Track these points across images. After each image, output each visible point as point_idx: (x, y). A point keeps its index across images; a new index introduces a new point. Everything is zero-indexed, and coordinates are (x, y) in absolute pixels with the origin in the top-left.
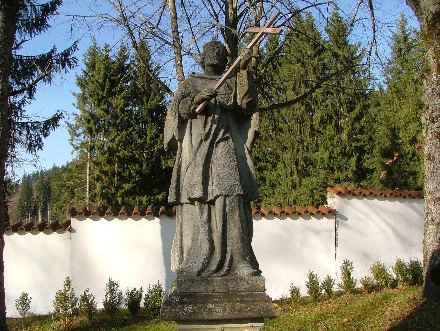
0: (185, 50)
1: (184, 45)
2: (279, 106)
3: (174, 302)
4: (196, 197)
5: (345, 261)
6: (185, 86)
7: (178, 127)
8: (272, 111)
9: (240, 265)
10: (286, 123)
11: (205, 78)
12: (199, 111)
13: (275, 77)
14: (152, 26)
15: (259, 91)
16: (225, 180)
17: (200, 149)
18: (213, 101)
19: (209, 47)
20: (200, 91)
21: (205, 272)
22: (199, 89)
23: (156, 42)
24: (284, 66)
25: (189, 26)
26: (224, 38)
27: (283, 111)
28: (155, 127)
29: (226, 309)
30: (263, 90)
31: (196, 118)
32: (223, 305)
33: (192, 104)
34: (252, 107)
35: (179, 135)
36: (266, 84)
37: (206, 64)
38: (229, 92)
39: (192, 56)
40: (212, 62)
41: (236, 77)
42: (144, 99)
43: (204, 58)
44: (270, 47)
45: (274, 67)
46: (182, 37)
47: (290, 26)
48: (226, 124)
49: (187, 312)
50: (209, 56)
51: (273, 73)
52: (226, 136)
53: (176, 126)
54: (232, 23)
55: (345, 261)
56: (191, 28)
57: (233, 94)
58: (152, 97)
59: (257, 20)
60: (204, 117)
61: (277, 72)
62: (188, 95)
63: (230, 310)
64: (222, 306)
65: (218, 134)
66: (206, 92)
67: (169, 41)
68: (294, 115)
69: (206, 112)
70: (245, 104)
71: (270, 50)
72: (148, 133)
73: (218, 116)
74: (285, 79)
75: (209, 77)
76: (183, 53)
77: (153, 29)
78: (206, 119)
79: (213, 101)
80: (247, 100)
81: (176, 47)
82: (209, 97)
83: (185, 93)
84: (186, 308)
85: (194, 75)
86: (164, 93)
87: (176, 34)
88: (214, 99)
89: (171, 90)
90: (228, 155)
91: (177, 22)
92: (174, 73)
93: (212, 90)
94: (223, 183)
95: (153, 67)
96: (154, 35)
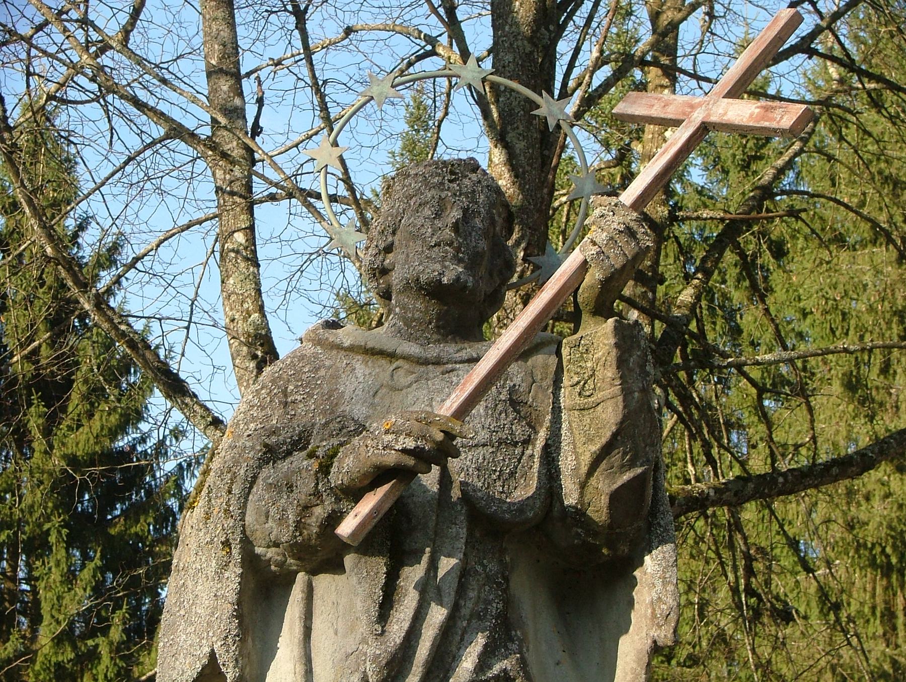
0: (274, 176)
1: (265, 144)
2: (769, 487)
6: (285, 393)
7: (239, 615)
8: (734, 515)
10: (809, 570)
11: (391, 356)
12: (354, 534)
13: (750, 319)
14: (94, 36)
15: (669, 405)
18: (430, 480)
19: (418, 192)
20: (361, 428)
22: (359, 411)
23: (117, 122)
24: (804, 259)
25: (298, 43)
26: (486, 114)
27: (792, 509)
28: (86, 575)
30: (686, 399)
31: (337, 567)
33: (317, 494)
34: (643, 516)
35: (242, 656)
36: (705, 358)
37: (396, 279)
38: (520, 431)
39: (309, 206)
40: (430, 271)
41: (558, 354)
42: (34, 422)
43: (389, 249)
44: (726, 154)
45: (748, 266)
46: (260, 102)
47: (837, 52)
48: (496, 607)
50: (414, 237)
51: (738, 296)
52: (496, 669)
53: (228, 609)
54: (531, 40)
56: (308, 53)
57: (540, 443)
58: (75, 401)
59: (664, 20)
60: (379, 566)
61: (760, 293)
62: (300, 443)
65: (456, 659)
66: (397, 433)
67: (189, 123)
68: (850, 526)
69: (392, 540)
70: (604, 500)
71: (726, 172)
72: (45, 608)
73: (453, 561)
74: (805, 327)
75: (412, 349)
76: (259, 188)
77: (103, 50)
78: (392, 577)
79: (430, 480)
80: (611, 476)
81: (224, 155)
82: (410, 461)
83: (284, 436)
85: (334, 336)
86: (144, 390)
87: (225, 85)
88: (435, 470)
89: (194, 387)
91: (232, 26)
92: (211, 291)
93: (428, 420)
95: (89, 245)
96: (107, 86)
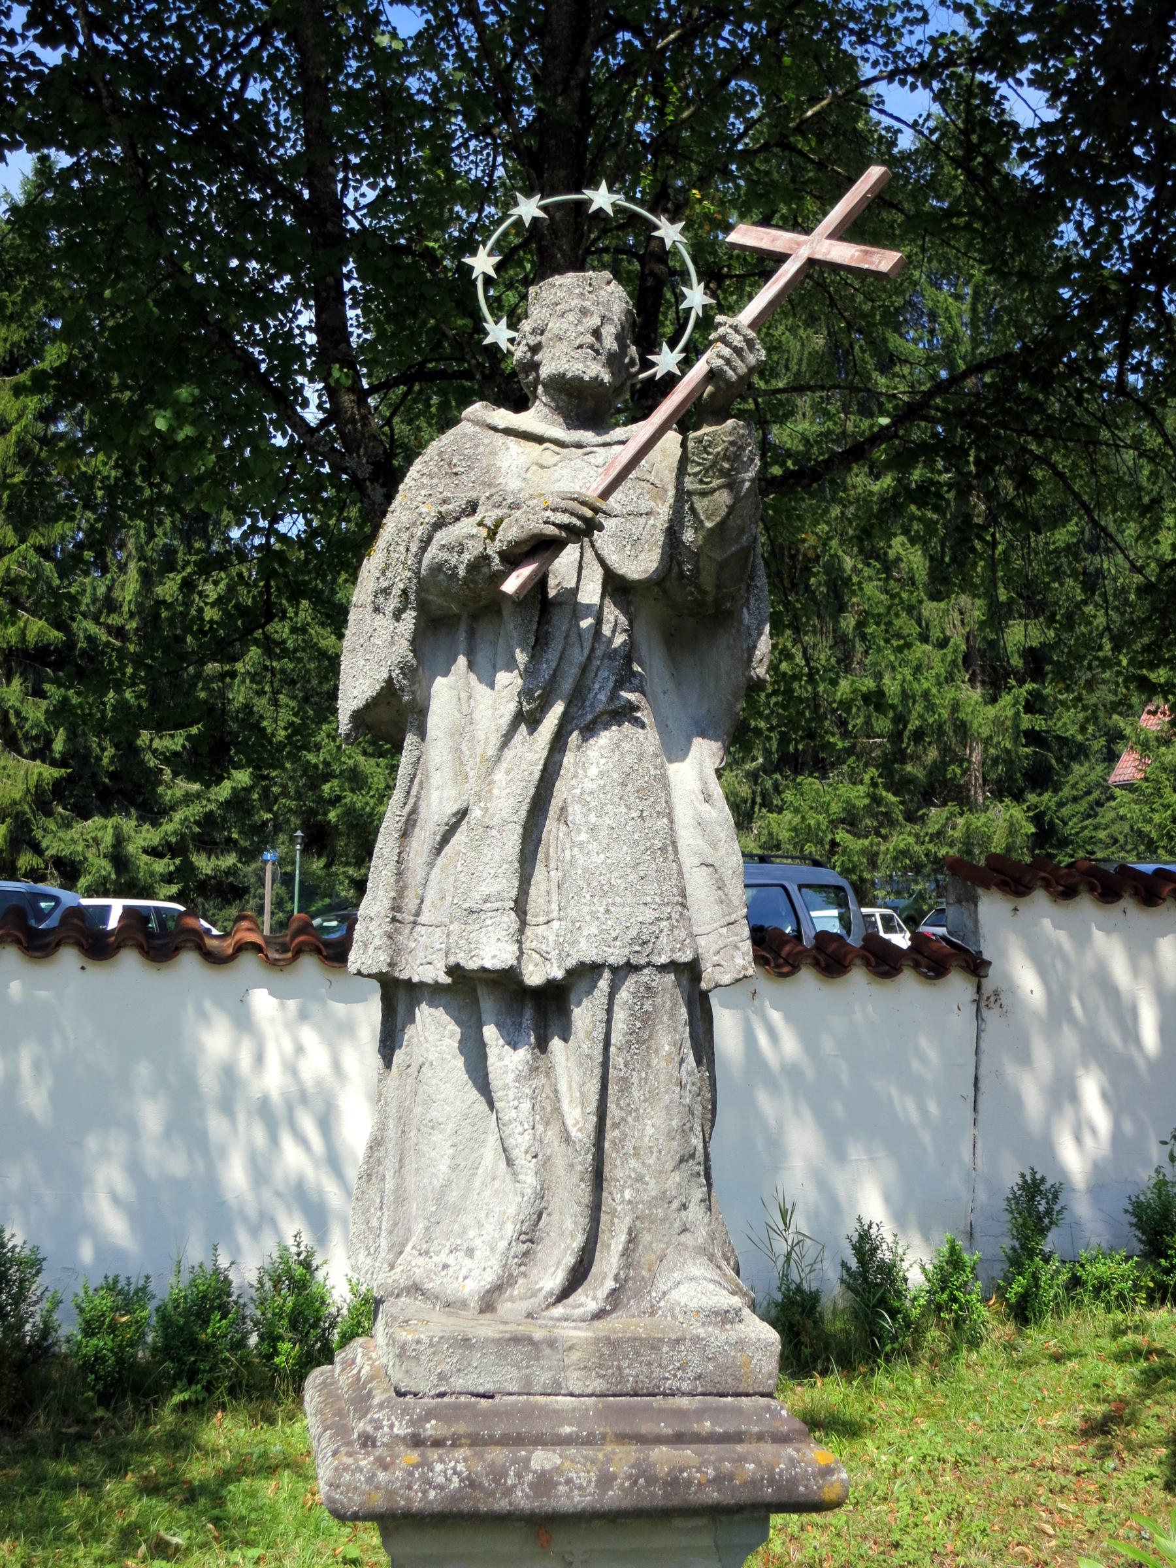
3: (382, 1436)
4: (488, 964)
5: (1028, 1178)
9: (672, 1270)
16: (618, 900)
17: (508, 753)
21: (512, 1299)
29: (614, 1477)
32: (600, 1456)
49: (441, 1488)
55: (1028, 1178)
63: (629, 1477)
64: (593, 1462)
84: (439, 1467)
90: (630, 788)
94: (608, 911)
